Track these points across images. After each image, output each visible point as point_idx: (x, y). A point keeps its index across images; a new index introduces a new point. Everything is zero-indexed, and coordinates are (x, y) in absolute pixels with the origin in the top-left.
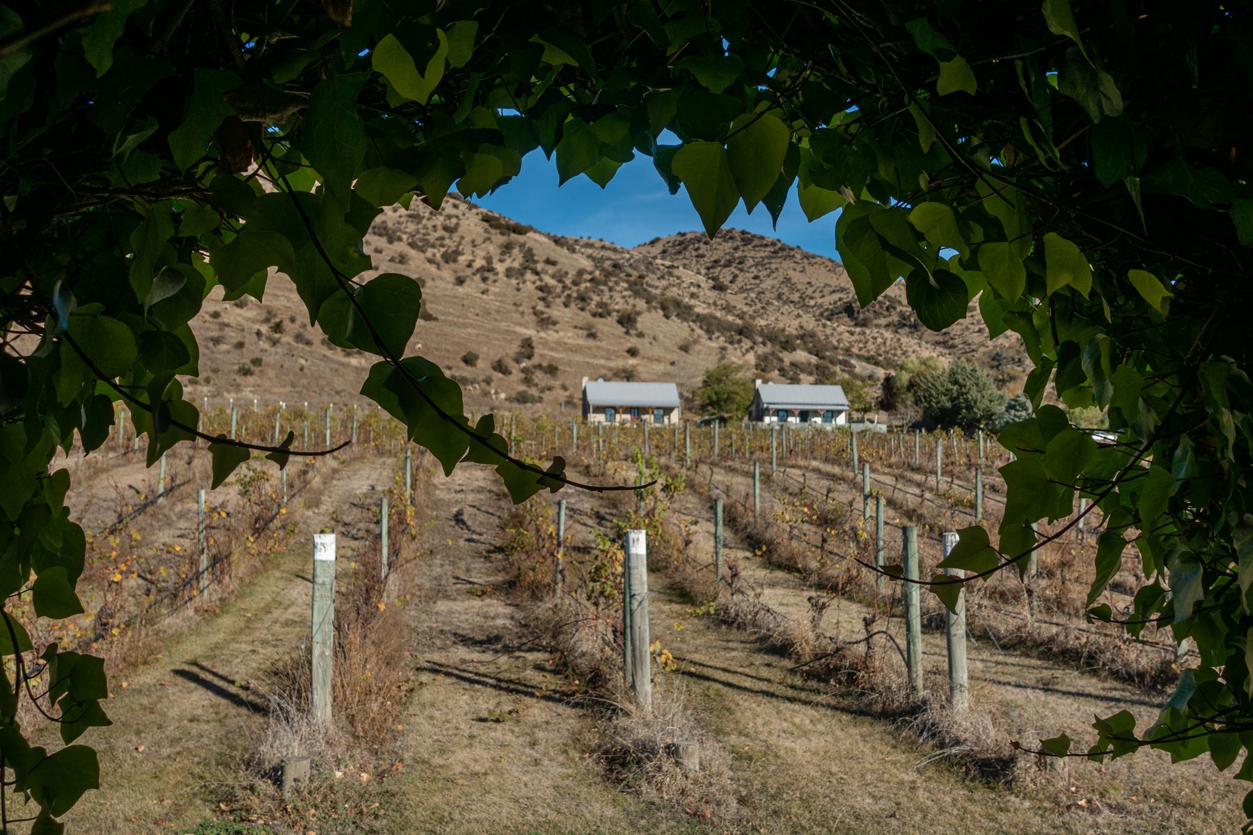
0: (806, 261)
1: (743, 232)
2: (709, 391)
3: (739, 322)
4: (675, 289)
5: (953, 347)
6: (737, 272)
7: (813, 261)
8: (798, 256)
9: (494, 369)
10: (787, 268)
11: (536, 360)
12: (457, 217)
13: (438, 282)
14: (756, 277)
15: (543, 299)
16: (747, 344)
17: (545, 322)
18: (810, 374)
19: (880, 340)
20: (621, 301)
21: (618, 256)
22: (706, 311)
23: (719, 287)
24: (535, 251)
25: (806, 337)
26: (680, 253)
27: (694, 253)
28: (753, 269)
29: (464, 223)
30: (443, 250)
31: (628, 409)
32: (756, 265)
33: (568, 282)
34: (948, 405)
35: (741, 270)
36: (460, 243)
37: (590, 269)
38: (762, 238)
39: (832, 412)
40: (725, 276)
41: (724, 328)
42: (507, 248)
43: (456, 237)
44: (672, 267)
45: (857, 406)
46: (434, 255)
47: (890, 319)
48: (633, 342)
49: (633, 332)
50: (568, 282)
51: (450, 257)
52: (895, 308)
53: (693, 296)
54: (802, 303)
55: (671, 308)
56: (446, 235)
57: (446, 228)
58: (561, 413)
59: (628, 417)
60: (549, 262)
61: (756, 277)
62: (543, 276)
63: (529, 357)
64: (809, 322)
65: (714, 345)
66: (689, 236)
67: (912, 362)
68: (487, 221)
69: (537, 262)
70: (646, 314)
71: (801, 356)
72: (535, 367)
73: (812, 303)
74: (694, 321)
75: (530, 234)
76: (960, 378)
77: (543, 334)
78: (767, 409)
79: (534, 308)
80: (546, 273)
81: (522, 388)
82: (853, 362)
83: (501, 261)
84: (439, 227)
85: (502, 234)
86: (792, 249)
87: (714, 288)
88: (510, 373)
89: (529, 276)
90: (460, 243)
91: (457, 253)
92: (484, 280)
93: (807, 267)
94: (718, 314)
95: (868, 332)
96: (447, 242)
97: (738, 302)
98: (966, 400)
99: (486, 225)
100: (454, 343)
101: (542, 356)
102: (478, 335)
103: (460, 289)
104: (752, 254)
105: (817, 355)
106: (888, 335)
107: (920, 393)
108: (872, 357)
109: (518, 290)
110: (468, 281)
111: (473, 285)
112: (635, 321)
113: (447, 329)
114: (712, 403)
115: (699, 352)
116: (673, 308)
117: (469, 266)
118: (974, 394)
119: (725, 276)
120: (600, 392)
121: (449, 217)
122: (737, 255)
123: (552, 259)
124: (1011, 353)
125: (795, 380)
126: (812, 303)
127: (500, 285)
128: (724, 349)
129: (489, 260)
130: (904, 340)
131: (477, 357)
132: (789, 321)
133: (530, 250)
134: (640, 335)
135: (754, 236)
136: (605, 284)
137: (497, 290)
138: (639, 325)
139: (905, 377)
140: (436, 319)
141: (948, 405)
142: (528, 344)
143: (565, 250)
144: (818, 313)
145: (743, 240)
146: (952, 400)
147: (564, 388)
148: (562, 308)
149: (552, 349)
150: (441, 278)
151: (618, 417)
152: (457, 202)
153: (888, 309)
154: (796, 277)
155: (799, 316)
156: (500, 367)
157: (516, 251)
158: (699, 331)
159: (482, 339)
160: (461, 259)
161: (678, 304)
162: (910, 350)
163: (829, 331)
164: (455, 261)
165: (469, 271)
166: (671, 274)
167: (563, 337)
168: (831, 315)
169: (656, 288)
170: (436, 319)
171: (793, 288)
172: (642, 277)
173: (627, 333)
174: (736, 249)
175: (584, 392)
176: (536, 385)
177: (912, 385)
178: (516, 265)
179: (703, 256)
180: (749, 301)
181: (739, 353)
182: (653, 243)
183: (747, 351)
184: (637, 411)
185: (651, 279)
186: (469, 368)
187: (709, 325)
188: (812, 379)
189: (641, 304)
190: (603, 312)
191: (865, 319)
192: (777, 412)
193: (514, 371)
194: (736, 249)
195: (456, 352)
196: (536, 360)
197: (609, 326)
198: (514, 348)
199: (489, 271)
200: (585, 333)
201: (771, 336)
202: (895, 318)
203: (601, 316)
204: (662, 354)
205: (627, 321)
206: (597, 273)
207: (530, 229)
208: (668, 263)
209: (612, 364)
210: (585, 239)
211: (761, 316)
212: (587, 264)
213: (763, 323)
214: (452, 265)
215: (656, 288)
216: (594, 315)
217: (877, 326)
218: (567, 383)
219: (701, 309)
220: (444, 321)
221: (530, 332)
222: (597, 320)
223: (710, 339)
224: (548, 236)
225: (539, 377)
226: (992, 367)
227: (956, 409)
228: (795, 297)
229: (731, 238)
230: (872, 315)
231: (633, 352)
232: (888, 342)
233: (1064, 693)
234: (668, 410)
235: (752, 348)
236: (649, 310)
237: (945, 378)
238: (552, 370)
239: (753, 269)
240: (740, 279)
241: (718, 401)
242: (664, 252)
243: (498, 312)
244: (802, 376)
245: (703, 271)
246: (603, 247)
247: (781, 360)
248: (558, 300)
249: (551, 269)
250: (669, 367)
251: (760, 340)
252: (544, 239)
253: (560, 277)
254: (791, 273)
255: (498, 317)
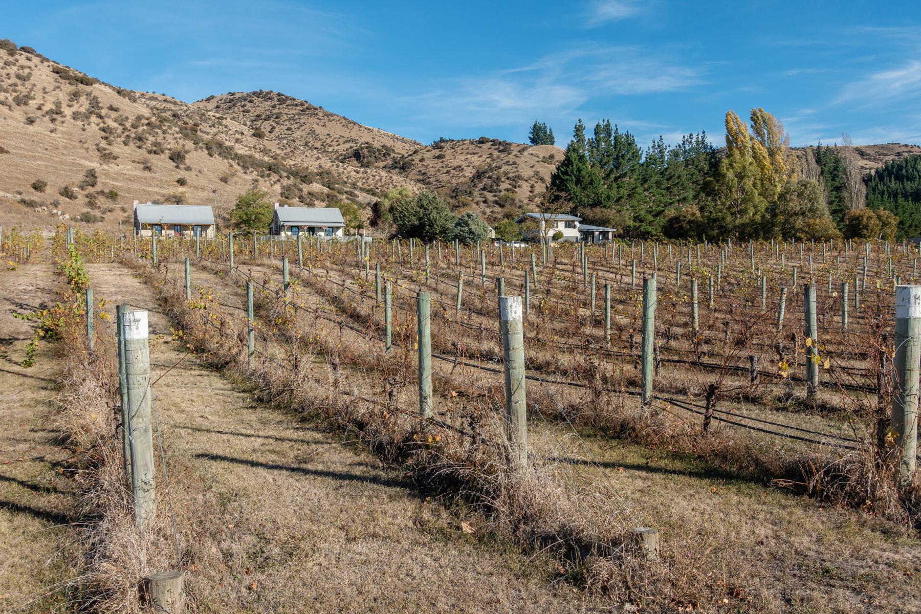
0: (326, 118)
1: (279, 95)
2: (241, 212)
3: (272, 161)
4: (223, 135)
5: (429, 183)
6: (274, 125)
7: (332, 118)
8: (321, 114)
9: (61, 194)
10: (312, 123)
11: (99, 187)
12: (30, 67)
13: (10, 121)
14: (289, 129)
15: (106, 138)
16: (274, 177)
17: (107, 157)
18: (323, 201)
19: (377, 177)
20: (173, 142)
21: (177, 108)
22: (248, 153)
23: (258, 134)
24: (100, 99)
25: (323, 175)
26: (230, 108)
27: (242, 109)
28: (287, 123)
29: (36, 73)
30: (15, 94)
31: (173, 226)
32: (289, 120)
33: (128, 125)
34: (417, 223)
35: (278, 123)
36: (31, 90)
37: (147, 115)
38: (294, 99)
39: (332, 227)
40: (265, 127)
41: (257, 165)
42: (75, 96)
43: (28, 84)
44: (221, 118)
45: (353, 224)
46: (7, 98)
47: (386, 163)
48: (182, 174)
49: (182, 166)
50: (128, 125)
51: (22, 101)
52: (389, 155)
53: (237, 141)
54: (323, 150)
55: (215, 148)
56: (19, 82)
57: (19, 77)
58: (120, 230)
59: (172, 233)
60: (111, 108)
61: (289, 129)
62: (106, 120)
63: (93, 185)
64: (326, 163)
65: (248, 177)
66: (237, 96)
67: (393, 193)
68: (57, 73)
69: (102, 108)
70: (193, 152)
71: (316, 187)
72: (98, 193)
73: (331, 149)
74: (232, 159)
75: (96, 86)
76: (424, 203)
77: (105, 167)
78: (283, 226)
79: (97, 145)
80: (109, 117)
81: (86, 210)
82: (357, 192)
83: (70, 106)
84: (13, 76)
85: (70, 83)
86: (316, 109)
87: (254, 135)
88: (76, 198)
89: (93, 119)
90: (31, 90)
91: (28, 97)
92: (53, 120)
93: (328, 123)
94: (257, 156)
95: (369, 171)
96: (20, 88)
97: (273, 146)
98: (429, 219)
99: (57, 76)
100: (25, 173)
101: (104, 184)
102: (46, 166)
103: (30, 127)
104: (286, 111)
105: (328, 187)
106: (383, 174)
107: (398, 215)
108: (372, 190)
109: (84, 130)
110: (38, 121)
111: (43, 125)
112: (184, 157)
113: (18, 161)
114: (244, 222)
115: (236, 183)
116: (215, 148)
117: (39, 109)
118: (434, 214)
119: (265, 127)
120: (148, 212)
121: (22, 67)
122: (274, 112)
123: (115, 106)
124: (465, 188)
125: (311, 205)
126: (331, 149)
127: (68, 125)
128: (256, 181)
129: (58, 104)
130: (395, 177)
131: (46, 185)
132: (311, 162)
133: (95, 98)
134: (188, 169)
135: (287, 98)
136: (160, 128)
137: (65, 129)
138: (187, 161)
139: (387, 204)
140: (7, 152)
141: (417, 223)
142: (92, 174)
143: (127, 99)
144: (335, 157)
145: (279, 100)
146: (420, 219)
147: (124, 210)
148: (122, 146)
149: (113, 179)
150: (12, 118)
151: (163, 232)
152: (29, 55)
153: (384, 155)
154: (319, 130)
155: (319, 158)
156: (66, 193)
157: (83, 99)
158: (236, 167)
159: (50, 169)
160: (32, 103)
161: (220, 145)
162: (399, 185)
163: (341, 170)
164: (26, 104)
165: (39, 113)
166: (220, 124)
167: (122, 171)
168: (344, 159)
169: (208, 134)
170: (7, 152)
171: (317, 138)
172: (196, 125)
173: (177, 167)
174: (274, 107)
175: (135, 212)
176: (99, 208)
177: (392, 209)
178: (83, 110)
179: (248, 111)
180: (281, 146)
181: (268, 184)
182: (208, 100)
183: (275, 183)
184: (180, 228)
185: (204, 126)
186: (38, 193)
187: (245, 162)
188: (324, 204)
189: (189, 145)
190: (157, 150)
191: (368, 163)
192: (291, 228)
193: (79, 196)
194: (274, 107)
195: (25, 180)
196: (99, 187)
197: (162, 162)
198: (80, 177)
199: (57, 113)
200: (142, 166)
201: (293, 173)
202: (390, 162)
203: (155, 153)
204: (206, 184)
205: (177, 157)
206: (154, 119)
207: (97, 81)
208: (218, 115)
209: (164, 191)
210: (150, 94)
211: (290, 158)
212: (146, 112)
213: (292, 163)
214: (23, 107)
215: (208, 134)
216: (150, 152)
217: (376, 167)
218: (126, 206)
219: (241, 150)
220: (15, 154)
221: (94, 165)
222: (153, 155)
223: (245, 173)
224: (114, 89)
225: (101, 201)
226: (452, 197)
227: (422, 226)
228: (318, 144)
229: (270, 98)
230: (373, 160)
231: (181, 182)
232: (384, 179)
233: (317, 473)
234: (205, 227)
235: (279, 181)
236: (196, 150)
237: (414, 203)
238: (113, 196)
239: (287, 123)
240: (277, 130)
241: (248, 220)
242: (218, 107)
243: (65, 148)
244: (316, 202)
245: (249, 123)
246: (165, 101)
247: (302, 190)
248: (118, 139)
249: (114, 115)
250: (211, 194)
251: (285, 174)
252: (110, 91)
253: (121, 121)
254: (315, 126)
255: (65, 152)
